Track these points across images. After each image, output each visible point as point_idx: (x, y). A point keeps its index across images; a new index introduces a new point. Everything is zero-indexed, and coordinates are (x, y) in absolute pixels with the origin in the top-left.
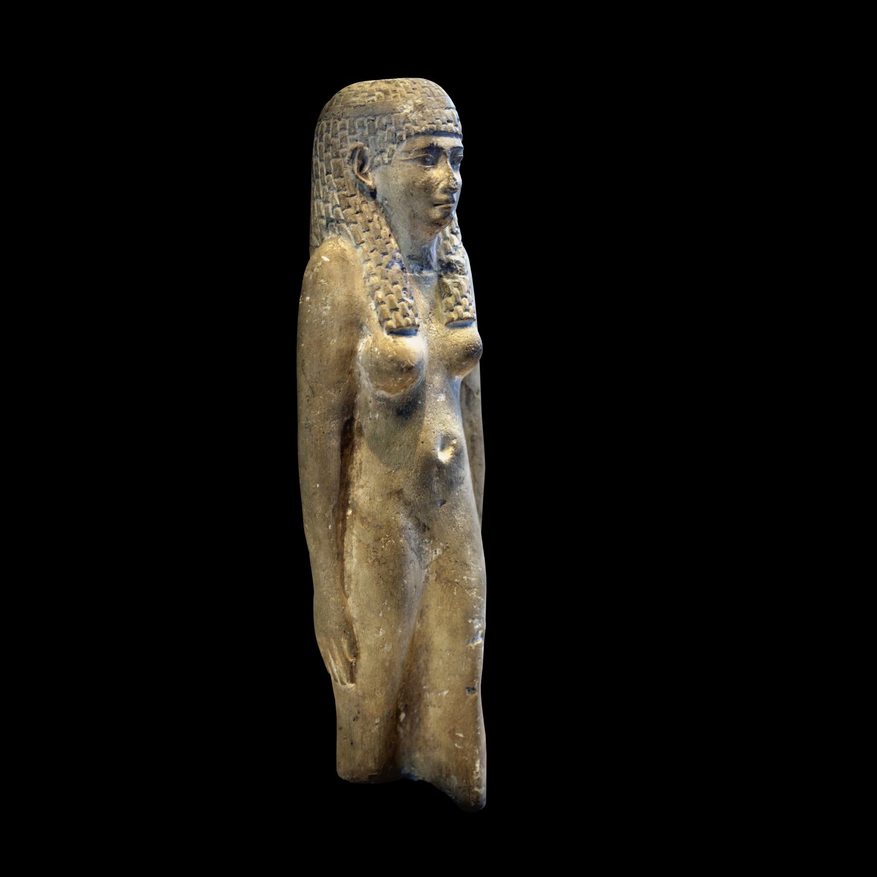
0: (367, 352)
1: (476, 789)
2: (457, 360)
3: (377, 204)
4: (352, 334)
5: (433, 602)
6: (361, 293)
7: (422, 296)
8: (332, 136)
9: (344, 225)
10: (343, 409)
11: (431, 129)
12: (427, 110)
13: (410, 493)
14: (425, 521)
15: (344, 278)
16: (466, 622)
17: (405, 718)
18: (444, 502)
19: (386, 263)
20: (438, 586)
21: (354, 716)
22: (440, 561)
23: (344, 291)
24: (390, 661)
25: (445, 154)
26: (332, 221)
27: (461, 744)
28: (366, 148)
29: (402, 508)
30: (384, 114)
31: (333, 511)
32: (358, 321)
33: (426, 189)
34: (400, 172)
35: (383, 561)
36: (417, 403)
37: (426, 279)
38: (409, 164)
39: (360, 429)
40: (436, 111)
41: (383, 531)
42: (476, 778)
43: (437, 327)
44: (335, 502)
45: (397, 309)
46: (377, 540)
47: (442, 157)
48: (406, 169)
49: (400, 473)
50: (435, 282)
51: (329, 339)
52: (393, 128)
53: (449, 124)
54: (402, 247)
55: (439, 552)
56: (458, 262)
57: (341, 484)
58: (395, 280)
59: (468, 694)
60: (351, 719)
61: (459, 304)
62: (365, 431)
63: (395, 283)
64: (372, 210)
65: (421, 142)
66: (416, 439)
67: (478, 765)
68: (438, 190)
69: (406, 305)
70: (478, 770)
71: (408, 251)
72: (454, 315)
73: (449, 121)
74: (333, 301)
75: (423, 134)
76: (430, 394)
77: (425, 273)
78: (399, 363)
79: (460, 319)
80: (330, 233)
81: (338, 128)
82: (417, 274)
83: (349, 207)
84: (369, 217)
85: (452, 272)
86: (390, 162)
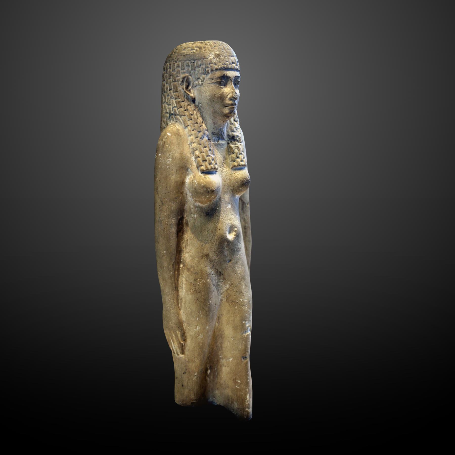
0: (190, 183)
1: (247, 409)
2: (237, 187)
3: (195, 106)
4: (183, 173)
5: (225, 313)
6: (187, 152)
7: (219, 154)
8: (172, 71)
9: (179, 117)
10: (178, 212)
11: (224, 67)
12: (222, 57)
13: (212, 256)
14: (221, 270)
15: (179, 144)
16: (242, 323)
17: (210, 373)
18: (230, 261)
19: (200, 136)
20: (227, 304)
21: (184, 371)
22: (228, 291)
23: (179, 151)
24: (202, 343)
25: (231, 80)
26: (172, 114)
27: (239, 386)
28: (190, 77)
29: (208, 263)
30: (199, 59)
31: (173, 265)
32: (186, 166)
33: (221, 98)
34: (207, 89)
35: (199, 291)
36: (216, 209)
37: (221, 145)
38: (212, 85)
39: (187, 223)
40: (226, 57)
41: (199, 276)
42: (247, 403)
43: (227, 170)
44: (174, 261)
45: (206, 160)
46: (196, 280)
47: (230, 81)
48: (211, 88)
49: (207, 245)
50: (226, 146)
51: (171, 176)
52: (204, 66)
53: (233, 64)
54: (209, 128)
55: (228, 286)
56: (238, 136)
57: (177, 251)
58: (205, 145)
59: (243, 360)
60: (182, 373)
61: (238, 158)
62: (189, 223)
63: (205, 147)
64: (193, 109)
65: (218, 74)
66: (216, 228)
67: (248, 397)
68: (227, 99)
69: (210, 158)
70: (248, 399)
71: (212, 130)
72: (236, 164)
73: (233, 63)
74: (173, 156)
75: (220, 69)
76: (223, 204)
77: (221, 142)
78: (207, 188)
79: (239, 165)
80: (171, 121)
81: (176, 66)
82: (216, 142)
83: (181, 107)
84: (191, 113)
85: (234, 141)
86: (202, 84)
